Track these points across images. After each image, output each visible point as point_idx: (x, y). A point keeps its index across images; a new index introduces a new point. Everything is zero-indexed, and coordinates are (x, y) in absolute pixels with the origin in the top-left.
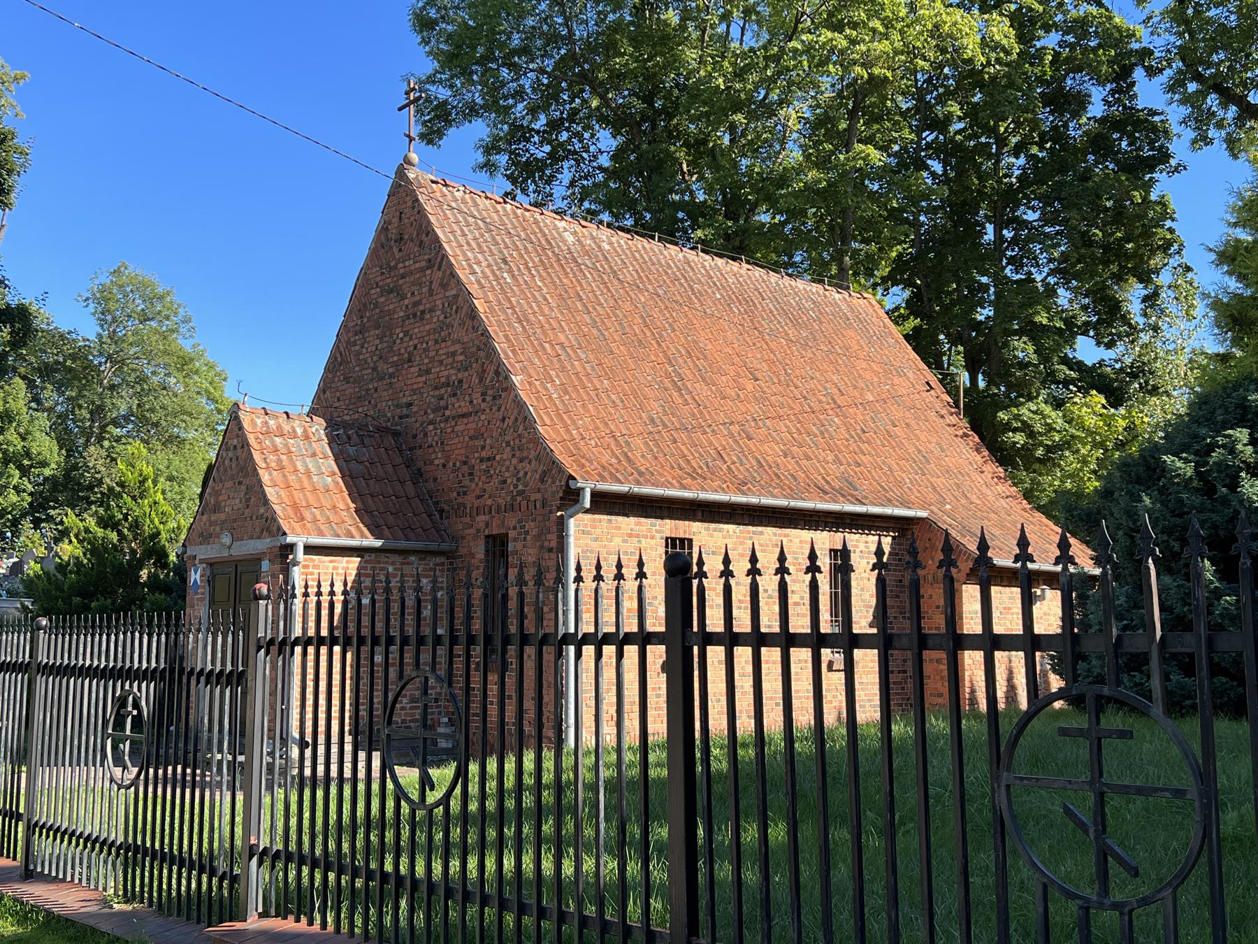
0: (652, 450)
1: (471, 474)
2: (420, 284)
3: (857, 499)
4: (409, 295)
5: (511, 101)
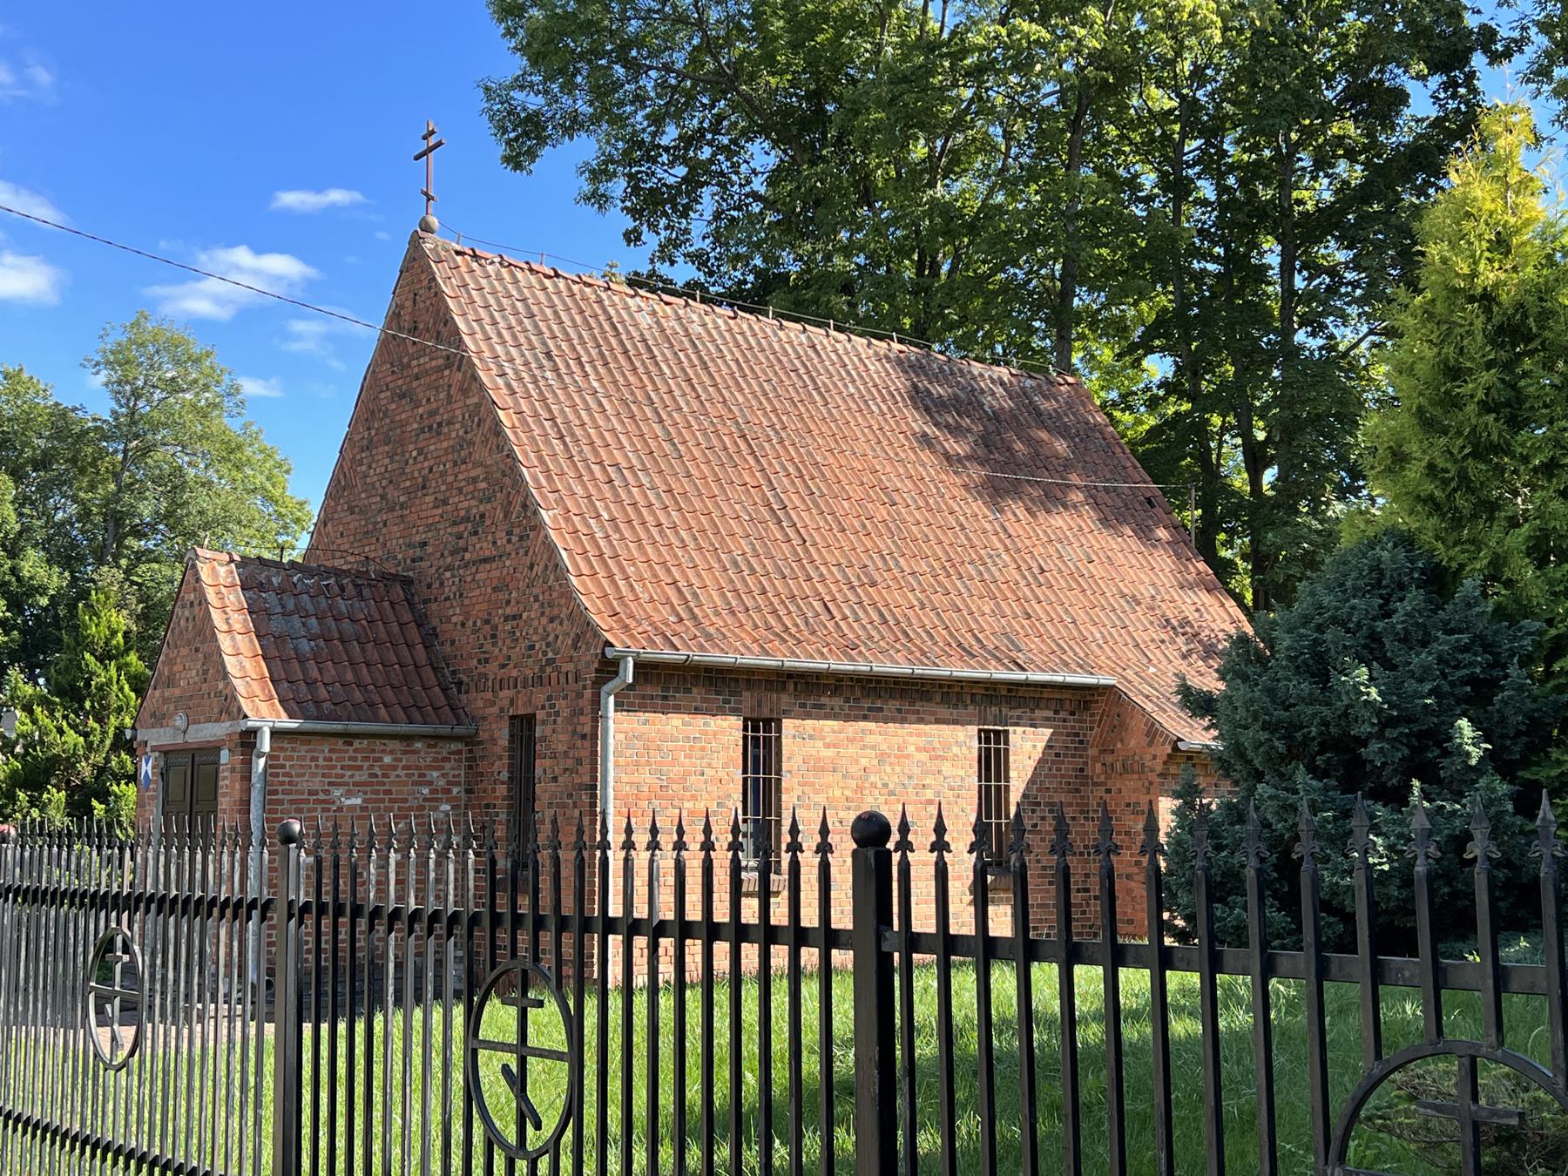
0: (729, 604)
1: (494, 636)
2: (437, 388)
4: (424, 402)
5: (628, 109)
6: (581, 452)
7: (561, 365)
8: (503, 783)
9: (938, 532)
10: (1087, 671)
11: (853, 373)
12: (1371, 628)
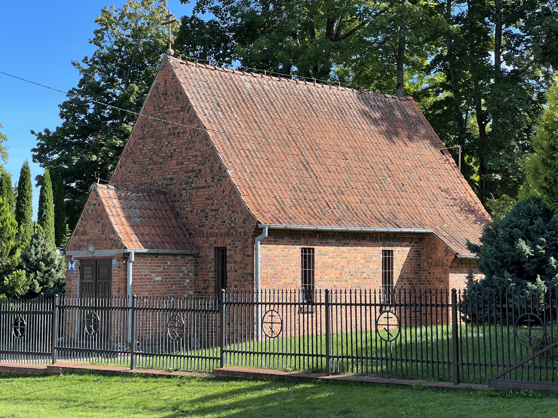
3: (397, 225)
6: (236, 145)
7: (223, 109)
8: (212, 272)
9: (364, 170)
10: (422, 227)
11: (325, 101)
12: (527, 228)
